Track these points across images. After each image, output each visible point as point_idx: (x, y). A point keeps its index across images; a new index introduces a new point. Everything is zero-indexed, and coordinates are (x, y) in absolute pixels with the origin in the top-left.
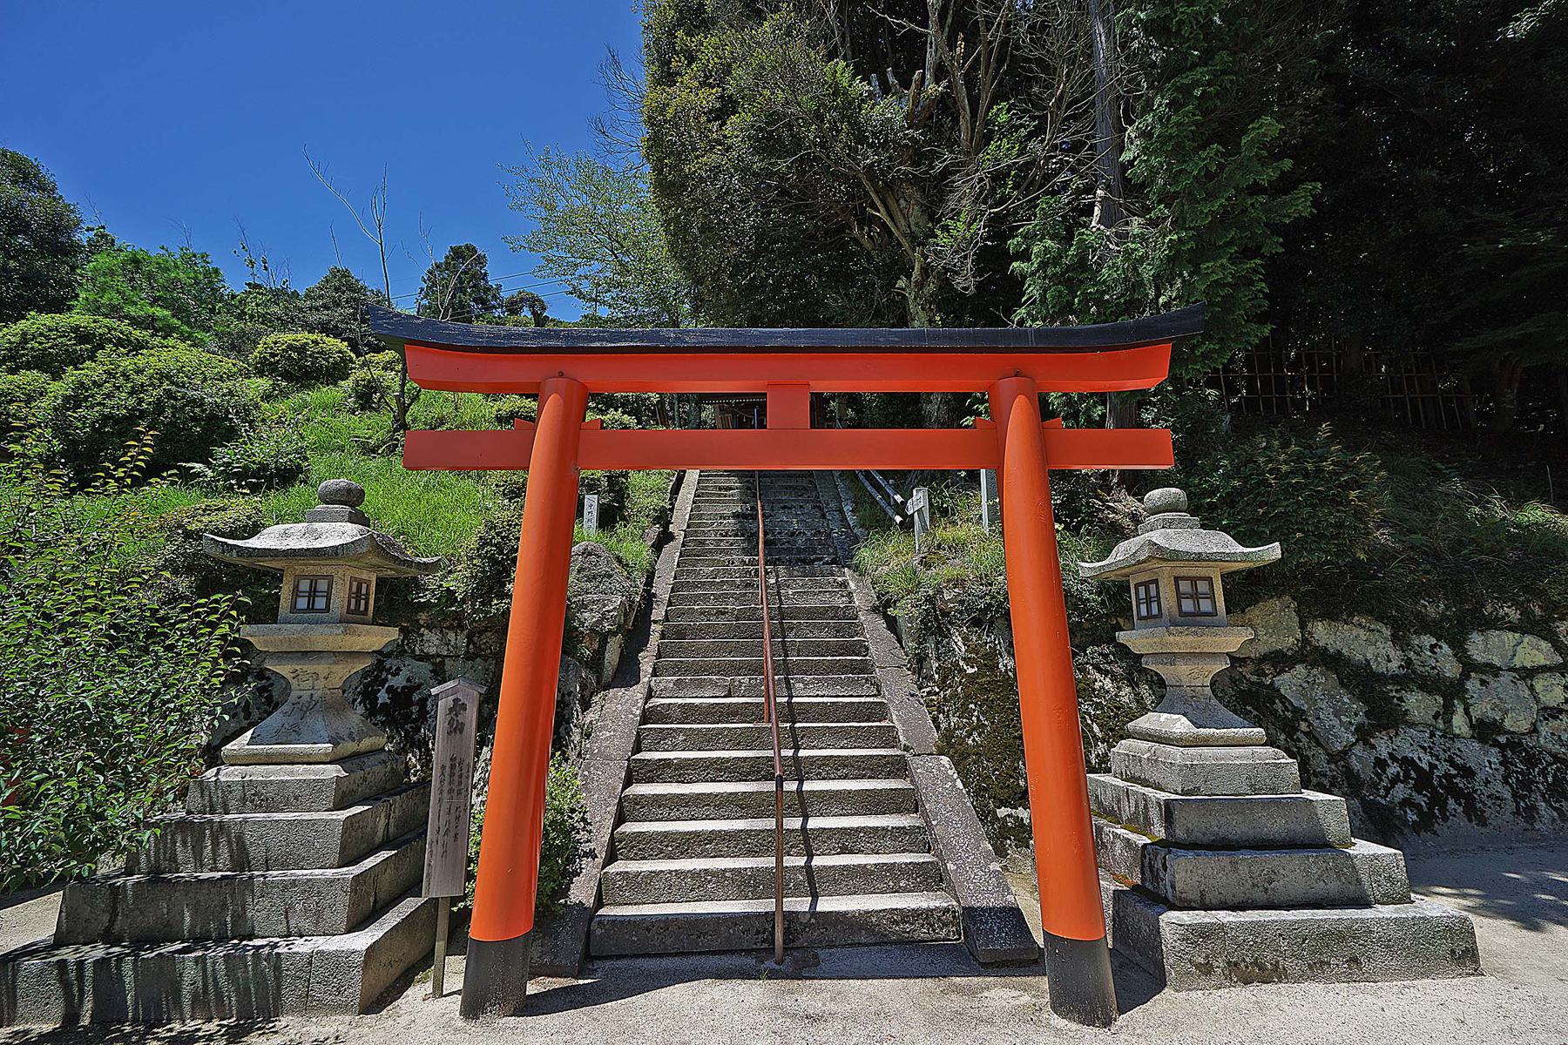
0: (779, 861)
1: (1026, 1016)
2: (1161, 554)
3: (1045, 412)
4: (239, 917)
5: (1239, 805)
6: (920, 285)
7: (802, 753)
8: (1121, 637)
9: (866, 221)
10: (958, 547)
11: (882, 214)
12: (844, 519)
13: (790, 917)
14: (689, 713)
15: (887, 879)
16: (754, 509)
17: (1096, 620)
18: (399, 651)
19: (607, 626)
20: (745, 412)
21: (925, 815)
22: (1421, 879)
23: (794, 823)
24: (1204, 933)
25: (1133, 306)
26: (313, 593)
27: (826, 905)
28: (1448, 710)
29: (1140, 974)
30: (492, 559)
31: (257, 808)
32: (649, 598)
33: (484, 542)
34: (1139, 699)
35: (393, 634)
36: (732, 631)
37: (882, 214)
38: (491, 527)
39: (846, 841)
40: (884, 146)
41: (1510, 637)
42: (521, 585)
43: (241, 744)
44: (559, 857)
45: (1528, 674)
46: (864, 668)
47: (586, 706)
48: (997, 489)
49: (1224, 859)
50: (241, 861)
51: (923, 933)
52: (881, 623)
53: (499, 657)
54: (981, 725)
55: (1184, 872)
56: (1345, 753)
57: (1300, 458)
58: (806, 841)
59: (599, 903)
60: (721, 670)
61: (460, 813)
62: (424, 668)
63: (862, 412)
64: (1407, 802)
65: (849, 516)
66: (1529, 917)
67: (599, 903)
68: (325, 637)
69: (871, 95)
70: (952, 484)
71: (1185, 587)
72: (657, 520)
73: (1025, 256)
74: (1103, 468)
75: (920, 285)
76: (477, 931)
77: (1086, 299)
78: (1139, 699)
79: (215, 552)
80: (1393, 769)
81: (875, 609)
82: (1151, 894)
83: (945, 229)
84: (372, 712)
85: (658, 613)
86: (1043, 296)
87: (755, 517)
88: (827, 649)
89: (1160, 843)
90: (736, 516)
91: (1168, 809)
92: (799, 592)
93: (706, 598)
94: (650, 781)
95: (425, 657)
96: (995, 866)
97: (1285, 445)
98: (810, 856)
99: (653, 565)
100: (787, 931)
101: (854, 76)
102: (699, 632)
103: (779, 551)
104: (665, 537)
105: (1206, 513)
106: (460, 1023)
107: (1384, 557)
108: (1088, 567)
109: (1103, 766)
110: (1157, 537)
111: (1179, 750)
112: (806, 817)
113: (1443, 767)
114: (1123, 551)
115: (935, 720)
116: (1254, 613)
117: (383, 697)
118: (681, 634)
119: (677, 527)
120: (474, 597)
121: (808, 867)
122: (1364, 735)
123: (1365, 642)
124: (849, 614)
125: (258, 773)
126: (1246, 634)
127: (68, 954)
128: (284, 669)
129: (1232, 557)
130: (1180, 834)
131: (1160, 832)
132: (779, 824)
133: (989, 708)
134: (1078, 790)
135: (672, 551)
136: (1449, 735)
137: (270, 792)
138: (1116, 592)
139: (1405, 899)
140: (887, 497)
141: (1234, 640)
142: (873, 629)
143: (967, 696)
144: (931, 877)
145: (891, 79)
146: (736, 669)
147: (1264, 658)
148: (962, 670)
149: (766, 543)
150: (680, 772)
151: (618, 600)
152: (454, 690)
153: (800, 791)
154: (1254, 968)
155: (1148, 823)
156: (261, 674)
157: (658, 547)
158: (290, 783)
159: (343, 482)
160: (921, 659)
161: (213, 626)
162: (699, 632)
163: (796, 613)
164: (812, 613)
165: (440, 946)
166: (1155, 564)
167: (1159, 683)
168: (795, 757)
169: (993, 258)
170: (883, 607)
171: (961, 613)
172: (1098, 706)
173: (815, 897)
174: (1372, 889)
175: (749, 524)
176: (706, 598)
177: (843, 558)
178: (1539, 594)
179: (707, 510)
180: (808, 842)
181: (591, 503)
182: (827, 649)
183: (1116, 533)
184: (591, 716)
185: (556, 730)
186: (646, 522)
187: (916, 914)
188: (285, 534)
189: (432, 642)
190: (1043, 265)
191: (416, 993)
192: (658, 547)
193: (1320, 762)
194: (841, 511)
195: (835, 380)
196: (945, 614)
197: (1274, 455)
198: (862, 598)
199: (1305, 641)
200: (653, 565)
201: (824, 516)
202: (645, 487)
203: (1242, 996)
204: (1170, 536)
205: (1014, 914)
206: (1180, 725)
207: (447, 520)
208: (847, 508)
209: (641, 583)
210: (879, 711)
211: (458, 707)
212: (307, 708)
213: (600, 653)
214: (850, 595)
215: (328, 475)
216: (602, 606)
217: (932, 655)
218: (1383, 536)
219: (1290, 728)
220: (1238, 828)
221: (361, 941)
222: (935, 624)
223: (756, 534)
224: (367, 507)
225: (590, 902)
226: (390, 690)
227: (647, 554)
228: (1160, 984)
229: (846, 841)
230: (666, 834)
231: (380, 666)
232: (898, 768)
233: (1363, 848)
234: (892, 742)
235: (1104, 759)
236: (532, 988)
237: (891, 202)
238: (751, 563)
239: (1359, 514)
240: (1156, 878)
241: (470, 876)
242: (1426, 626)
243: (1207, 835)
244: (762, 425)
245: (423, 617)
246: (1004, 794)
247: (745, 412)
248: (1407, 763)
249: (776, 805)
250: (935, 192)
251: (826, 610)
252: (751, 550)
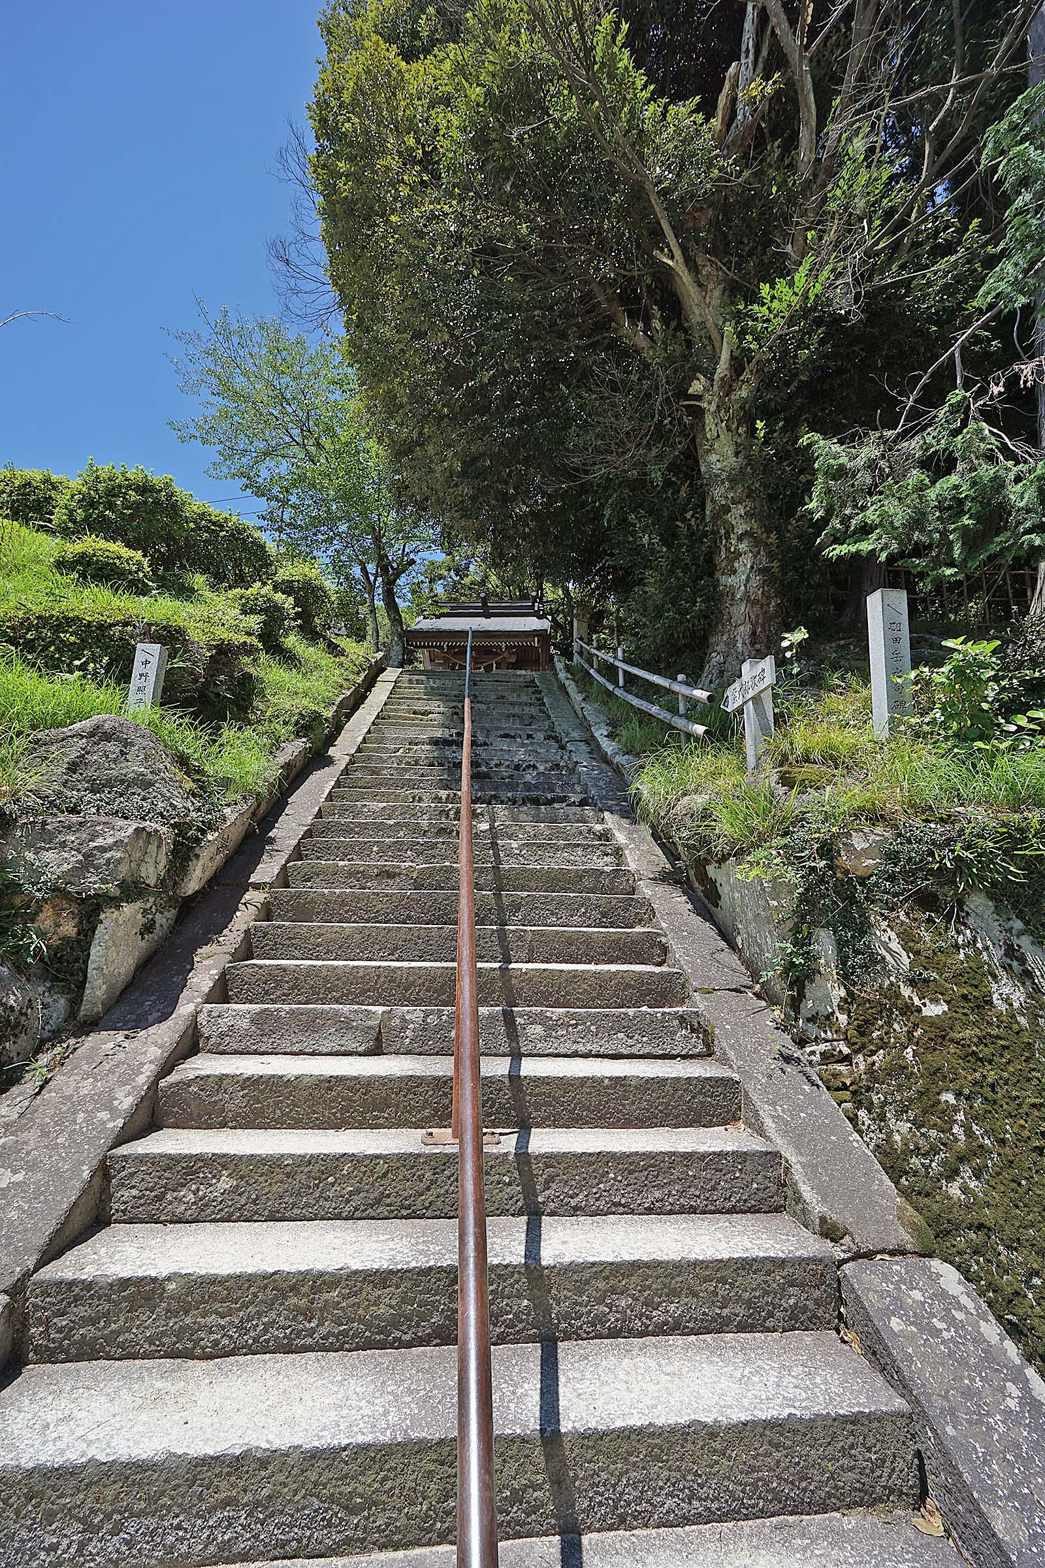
6: (728, 387)
36: (401, 911)
75: (728, 387)
87: (460, 744)
90: (435, 742)
92: (523, 839)
101: (539, 578)
118: (303, 911)
119: (341, 751)
124: (619, 882)
140: (668, 699)
148: (908, 1010)
160: (800, 978)
163: (524, 880)
164: (555, 881)
171: (891, 878)
201: (563, 748)
214: (618, 852)
223: (458, 765)
251: (580, 876)
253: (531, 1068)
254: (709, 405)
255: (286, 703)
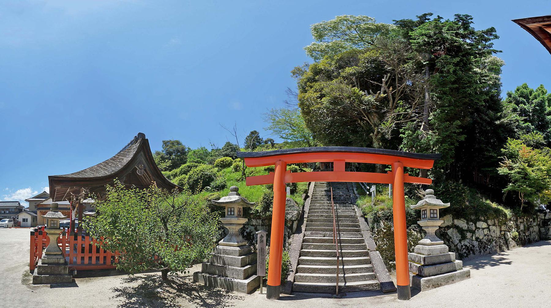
0: (338, 275)
1: (394, 300)
2: (428, 204)
3: (405, 170)
4: (225, 273)
5: (437, 256)
6: (376, 135)
7: (343, 251)
8: (418, 222)
9: (361, 119)
10: (383, 201)
11: (367, 119)
12: (354, 192)
13: (340, 287)
14: (314, 241)
15: (364, 278)
16: (330, 189)
17: (413, 219)
18: (247, 224)
19: (294, 219)
20: (328, 166)
21: (373, 264)
22: (464, 265)
23: (341, 267)
24: (429, 281)
25: (427, 149)
26: (231, 211)
27: (348, 284)
28: (473, 236)
29: (416, 289)
30: (266, 202)
31: (226, 254)
32: (303, 212)
33: (264, 198)
34: (421, 236)
35: (246, 220)
37: (367, 119)
38: (265, 195)
39: (354, 271)
40: (368, 105)
41: (482, 222)
42: (275, 209)
43: (221, 242)
44: (285, 270)
45: (483, 229)
46: (359, 231)
47: (289, 238)
48: (392, 188)
49: (434, 267)
50: (224, 263)
51: (371, 288)
52: (363, 219)
53: (270, 226)
54: (387, 244)
55: (426, 270)
56: (457, 245)
57: (456, 186)
58: (344, 271)
59: (294, 281)
60: (322, 230)
61: (263, 260)
62: (253, 228)
63: (360, 168)
64: (465, 253)
65: (355, 191)
66: (477, 268)
67: (294, 281)
68: (234, 220)
69: (365, 94)
70: (381, 187)
71: (432, 211)
72: (305, 192)
73: (404, 134)
74: (419, 183)
75: (376, 135)
76: (268, 283)
77: (417, 145)
78: (421, 236)
79: (214, 203)
80: (464, 247)
81: (362, 216)
82: (420, 275)
83: (384, 124)
84: (243, 237)
85: (306, 216)
86: (407, 143)
87: (330, 191)
88: (349, 226)
89: (423, 266)
90: (325, 191)
91: (424, 259)
92: (342, 210)
93: (318, 212)
94: (305, 256)
95: (253, 225)
96: (388, 274)
97: (454, 183)
98: (345, 274)
99: (304, 203)
100: (339, 289)
102: (316, 221)
103: (337, 200)
104: (307, 197)
105: (438, 195)
106: (267, 299)
107: (467, 207)
108: (412, 206)
109: (413, 251)
110: (427, 200)
111: (430, 246)
112: (344, 266)
113: (471, 246)
114: (420, 203)
115: (376, 243)
116: (445, 217)
117: (245, 234)
119: (310, 194)
120: (262, 212)
121: (344, 277)
122: (460, 241)
123: (462, 223)
125: (225, 247)
126: (442, 222)
127: (203, 274)
128: (227, 227)
129: (441, 205)
130: (426, 263)
131: (422, 263)
132: (338, 267)
133: (389, 240)
134: (406, 255)
135: (309, 200)
136: (472, 240)
137: (227, 251)
138: (418, 213)
139: (462, 269)
141: (440, 223)
142: (361, 221)
143: (384, 237)
144: (374, 277)
145: (371, 92)
146: (326, 230)
147: (446, 227)
149: (333, 198)
150: (313, 254)
151: (296, 212)
152: (261, 233)
153: (342, 260)
154: (437, 285)
155: (420, 262)
156: (223, 228)
157: (305, 199)
158: (231, 250)
159: (234, 186)
160: (373, 228)
161: (216, 218)
162: (316, 221)
163: (341, 217)
165: (261, 285)
166: (426, 206)
167: (425, 233)
168: (341, 252)
169: (396, 133)
170: (364, 215)
172: (413, 238)
173: (346, 283)
174: (457, 268)
175: (328, 193)
176: (318, 212)
177: (353, 203)
178: (486, 215)
179: (318, 189)
180: (344, 271)
181: (288, 189)
182: (349, 226)
183: (420, 198)
184: (290, 240)
185: (283, 244)
186: (302, 193)
187: (369, 285)
188: (225, 199)
189: (254, 222)
190: (408, 136)
191: (257, 293)
192: (305, 199)
193: (453, 247)
194: (353, 190)
195: (355, 159)
196: (379, 217)
197: (452, 185)
198: (359, 213)
199: (453, 223)
200: (304, 203)
202: (301, 186)
203: (434, 290)
204: (430, 201)
205: (392, 283)
206: (428, 241)
207: (256, 194)
208: (355, 189)
209: (301, 208)
210: (362, 241)
211: (262, 237)
212: (232, 235)
213: (292, 225)
214: (355, 212)
215: (231, 185)
216: (292, 214)
217: (376, 227)
218: (467, 203)
219: (448, 241)
220: (437, 261)
221: (247, 281)
222: (377, 220)
224: (239, 192)
225: (292, 281)
226: (247, 232)
227: (302, 201)
228: (419, 290)
229: (354, 271)
230: (309, 268)
231: (244, 227)
232: (367, 254)
233: (457, 261)
234: (365, 248)
235: (413, 250)
236: (281, 295)
237: (369, 117)
238: (330, 203)
239: (464, 199)
240: (421, 272)
241: (266, 273)
242: (472, 221)
243: (433, 264)
244: (332, 170)
245: (252, 216)
246: (391, 259)
247: (328, 166)
248: (466, 246)
249: (337, 263)
250: (382, 117)
252: (329, 200)
253: (343, 251)
254: (374, 137)
255: (301, 188)
